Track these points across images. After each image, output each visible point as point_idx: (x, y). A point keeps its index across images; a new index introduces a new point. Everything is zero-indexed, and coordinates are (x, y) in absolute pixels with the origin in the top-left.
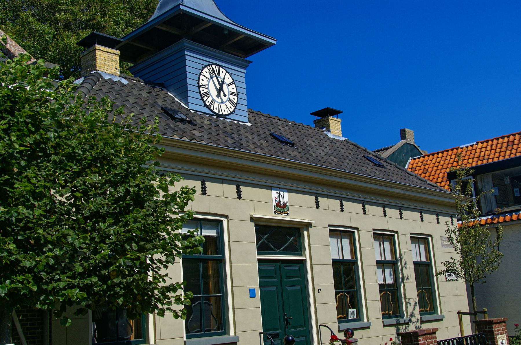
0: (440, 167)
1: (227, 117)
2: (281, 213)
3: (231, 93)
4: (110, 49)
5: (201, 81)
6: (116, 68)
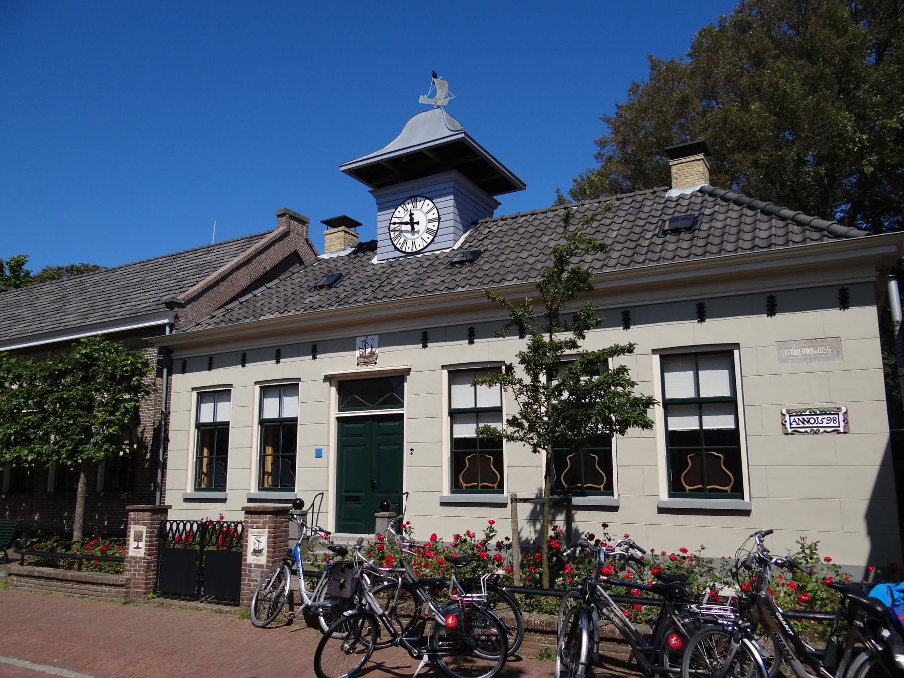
2: (365, 363)
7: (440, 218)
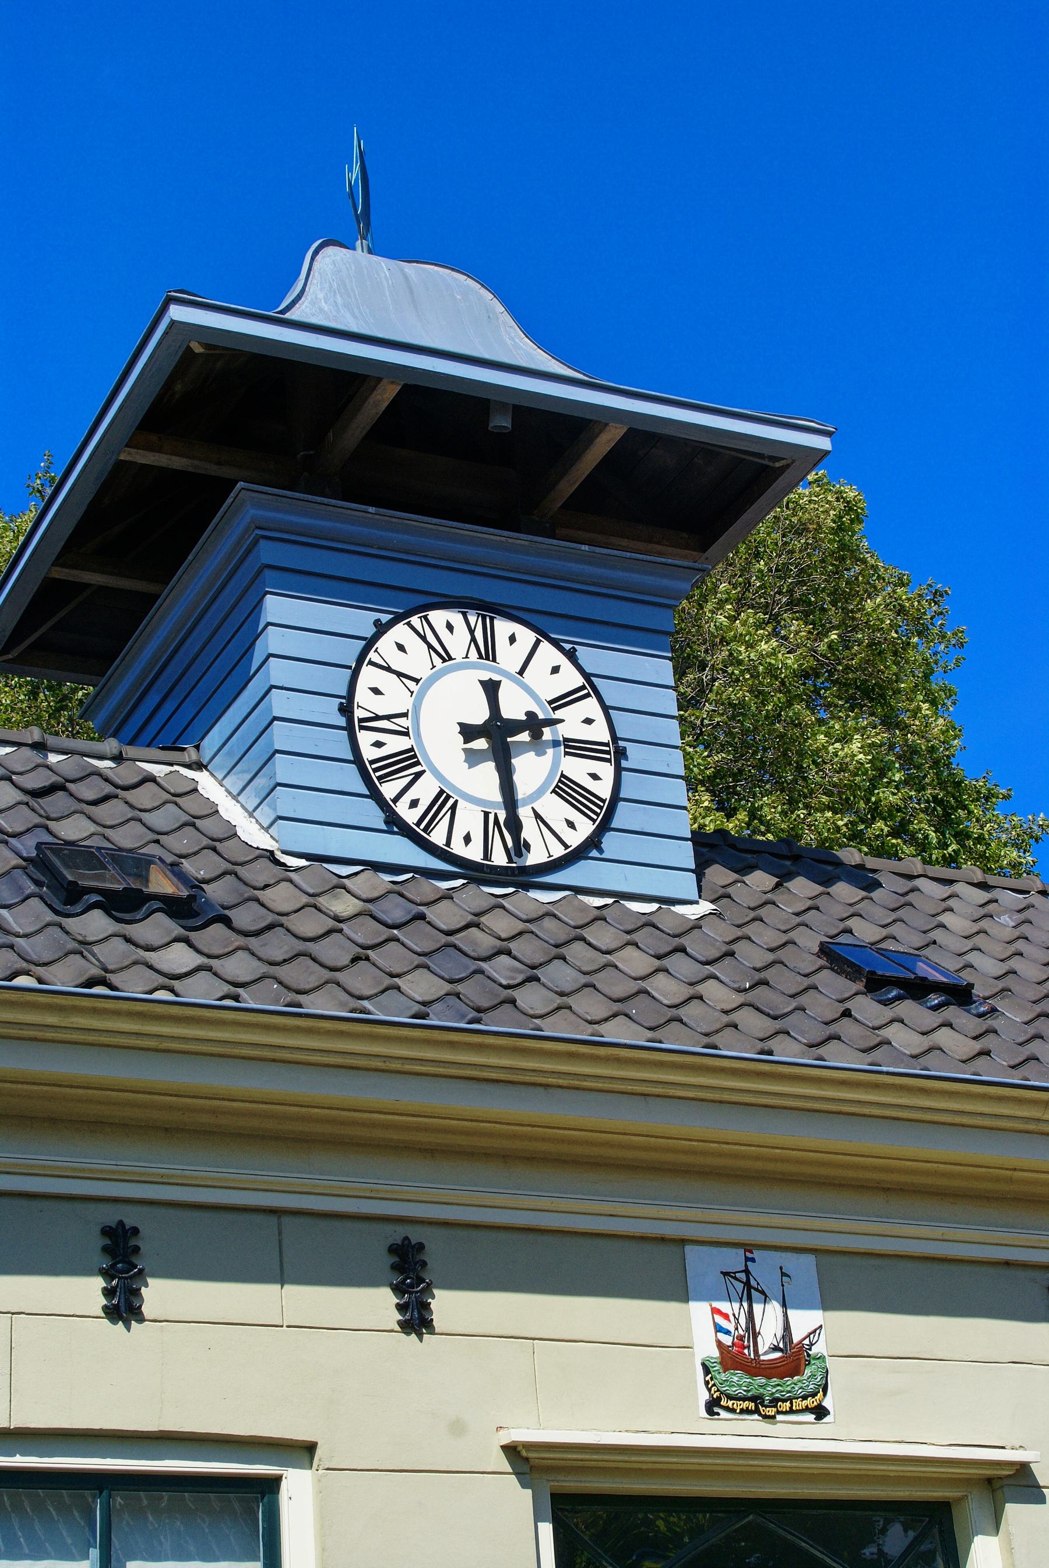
2: (758, 1405)
5: (362, 695)
7: (621, 754)
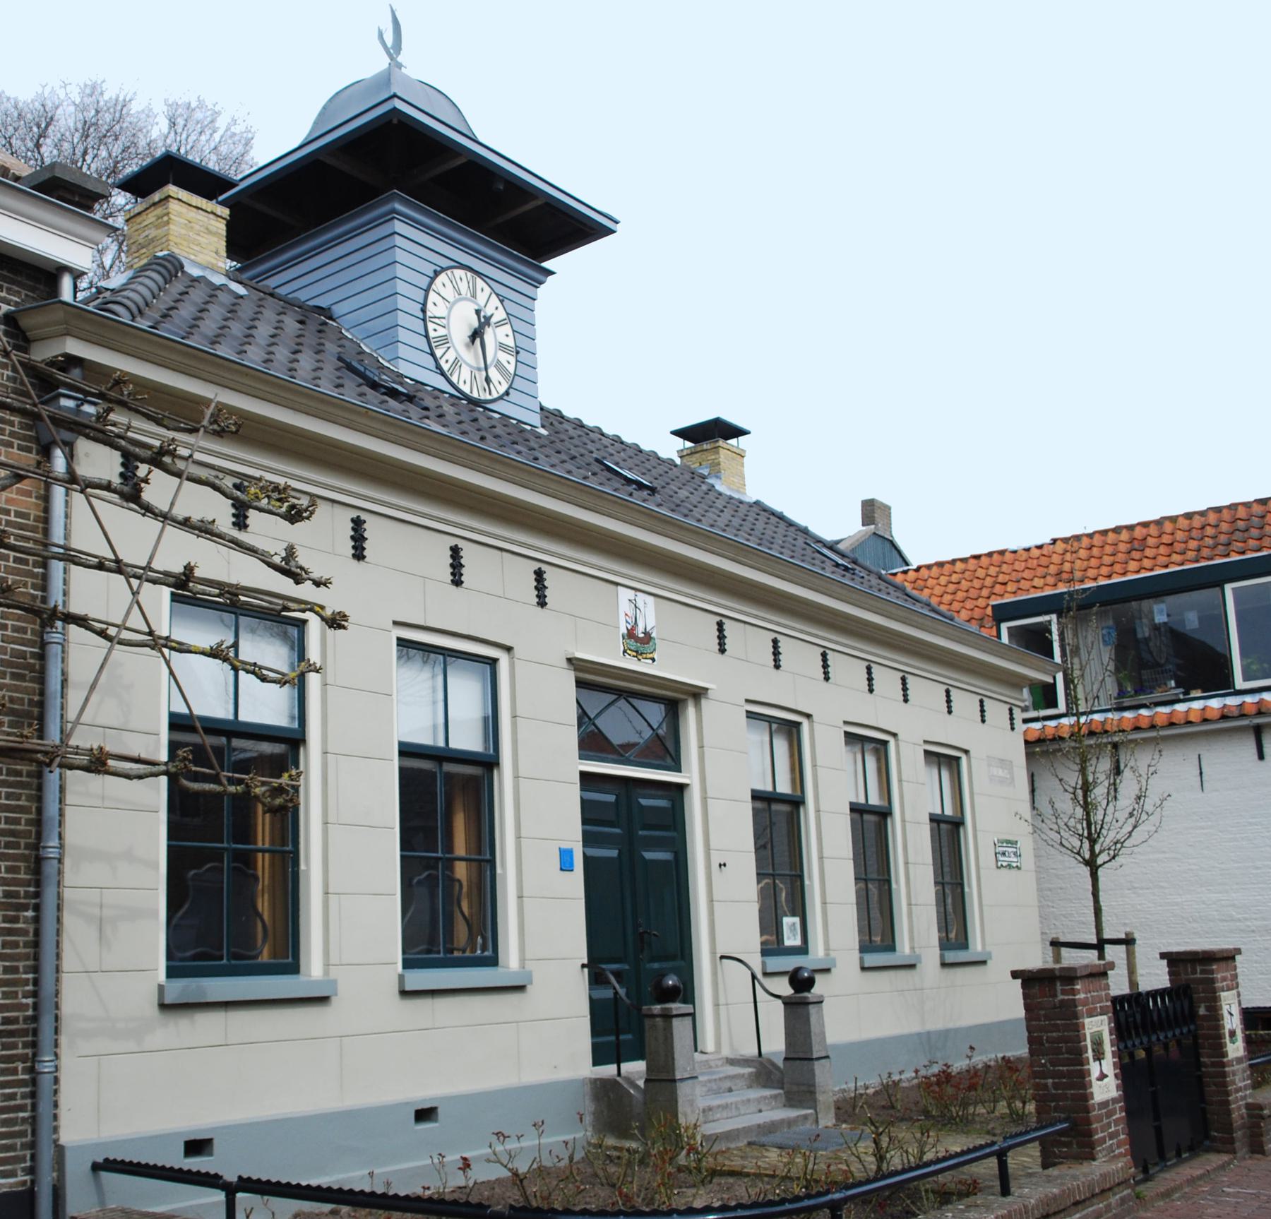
0: (960, 595)
1: (489, 406)
2: (638, 654)
3: (502, 347)
4: (205, 201)
5: (430, 306)
6: (217, 253)
